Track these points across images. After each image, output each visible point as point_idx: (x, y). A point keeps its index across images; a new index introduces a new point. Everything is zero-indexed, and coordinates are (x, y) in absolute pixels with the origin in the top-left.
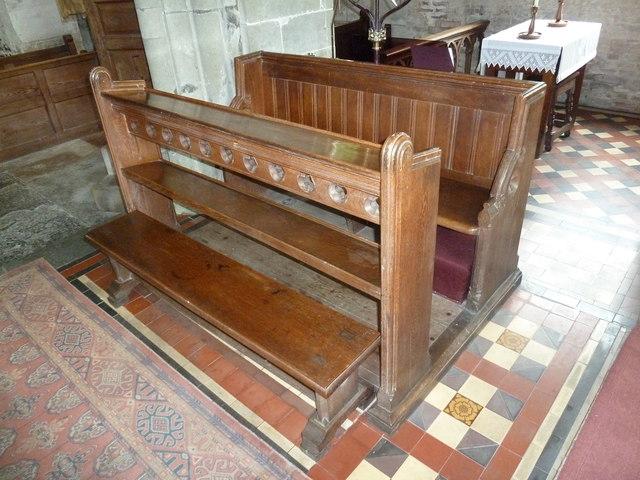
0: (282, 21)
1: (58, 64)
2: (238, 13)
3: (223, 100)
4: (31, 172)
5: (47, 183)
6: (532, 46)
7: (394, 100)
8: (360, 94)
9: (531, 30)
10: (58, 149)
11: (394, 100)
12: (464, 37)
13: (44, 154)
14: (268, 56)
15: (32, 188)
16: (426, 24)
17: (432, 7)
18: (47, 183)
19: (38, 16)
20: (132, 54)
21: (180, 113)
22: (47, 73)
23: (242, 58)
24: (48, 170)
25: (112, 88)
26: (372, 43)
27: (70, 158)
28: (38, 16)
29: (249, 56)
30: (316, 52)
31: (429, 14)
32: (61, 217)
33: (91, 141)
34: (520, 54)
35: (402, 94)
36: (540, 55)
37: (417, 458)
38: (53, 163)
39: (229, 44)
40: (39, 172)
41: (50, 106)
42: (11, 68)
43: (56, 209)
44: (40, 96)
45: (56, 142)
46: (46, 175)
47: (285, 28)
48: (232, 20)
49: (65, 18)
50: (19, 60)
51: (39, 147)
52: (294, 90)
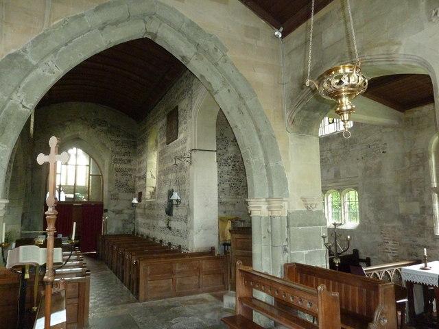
0: (305, 252)
1: (209, 259)
2: (288, 248)
3: (279, 276)
4: (187, 303)
5: (194, 309)
6: (425, 273)
7: (343, 285)
8: (331, 282)
9: (426, 266)
10: (199, 296)
11: (343, 285)
12: (395, 269)
13: (193, 297)
14: (297, 264)
15: (188, 310)
16: (388, 259)
17: (390, 251)
18: (194, 309)
19: (205, 238)
20: (248, 258)
21: (259, 299)
22: (204, 262)
23: (288, 264)
24: (195, 304)
25: (242, 268)
26: (335, 264)
27: (204, 300)
28: (205, 238)
29: (290, 264)
30: (319, 265)
31: (389, 254)
32: (201, 323)
33: (215, 296)
34: (408, 274)
35: (346, 283)
36: (417, 275)
37: (171, 55)
38: (196, 301)
39: (283, 259)
40: (191, 304)
41: (201, 276)
42: (188, 258)
43: (198, 319)
44: (199, 270)
45: (198, 293)
46: (194, 306)
47: (306, 255)
48: (286, 250)
49: (47, 164)
50: (192, 255)
51: (191, 294)
52: (306, 278)
